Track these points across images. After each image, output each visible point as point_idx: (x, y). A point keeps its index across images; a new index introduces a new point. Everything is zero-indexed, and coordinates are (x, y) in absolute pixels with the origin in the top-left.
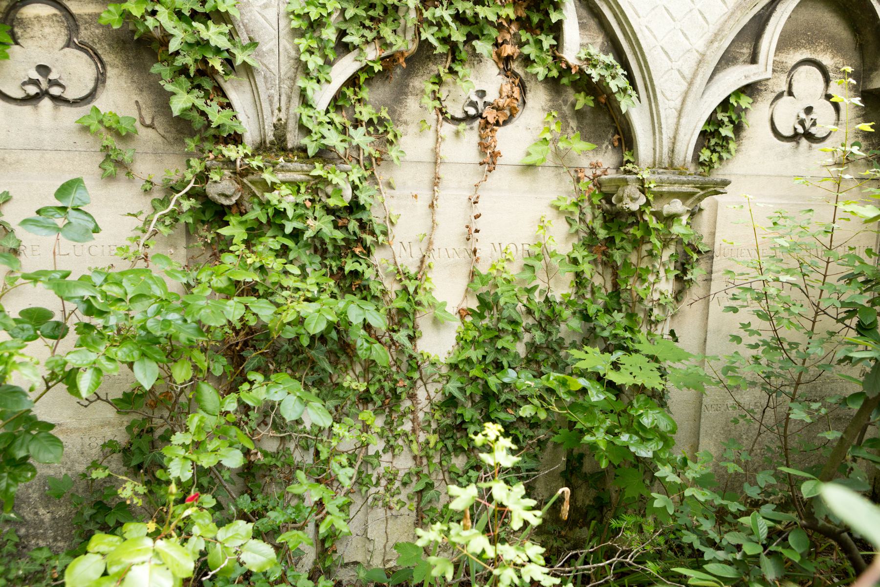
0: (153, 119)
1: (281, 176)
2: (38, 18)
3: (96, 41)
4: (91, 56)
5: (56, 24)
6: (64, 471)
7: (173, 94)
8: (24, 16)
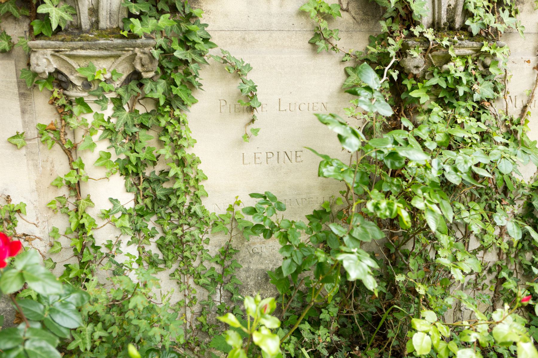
0: (348, 4)
1: (458, 52)
6: (271, 266)
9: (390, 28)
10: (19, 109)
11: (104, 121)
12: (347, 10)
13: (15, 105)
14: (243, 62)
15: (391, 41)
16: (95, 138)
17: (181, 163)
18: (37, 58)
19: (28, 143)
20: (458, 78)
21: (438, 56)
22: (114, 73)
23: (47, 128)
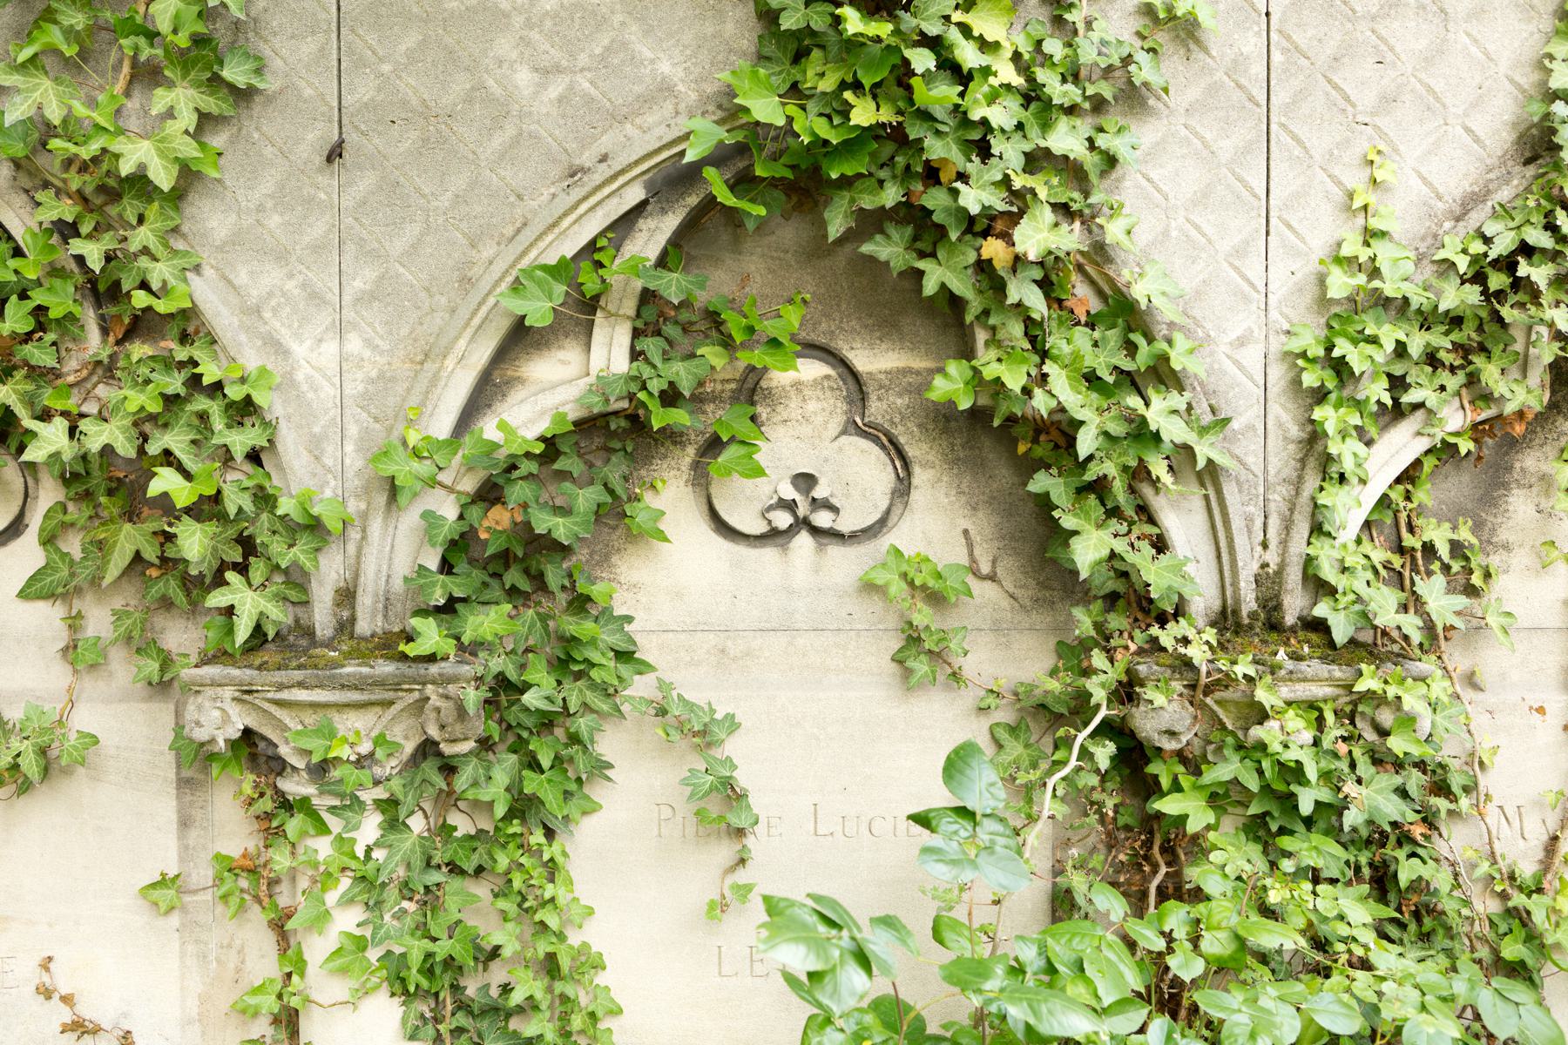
0: (994, 562)
1: (1286, 691)
2: (797, 385)
3: (897, 420)
4: (883, 447)
5: (828, 393)
7: (1076, 533)
8: (774, 384)
9: (1098, 626)
10: (174, 817)
11: (355, 858)
12: (992, 577)
13: (166, 808)
14: (713, 711)
15: (1098, 659)
16: (332, 898)
17: (550, 967)
18: (199, 708)
19: (187, 898)
20: (1292, 764)
21: (1236, 703)
22: (380, 741)
23: (234, 865)
